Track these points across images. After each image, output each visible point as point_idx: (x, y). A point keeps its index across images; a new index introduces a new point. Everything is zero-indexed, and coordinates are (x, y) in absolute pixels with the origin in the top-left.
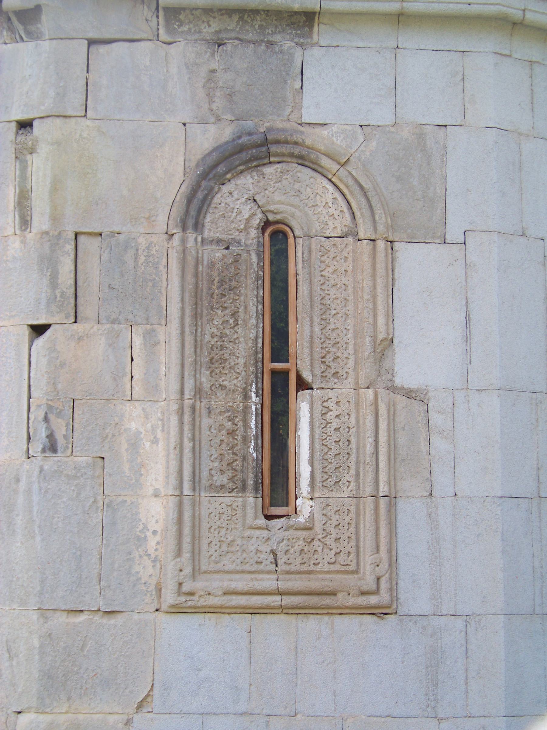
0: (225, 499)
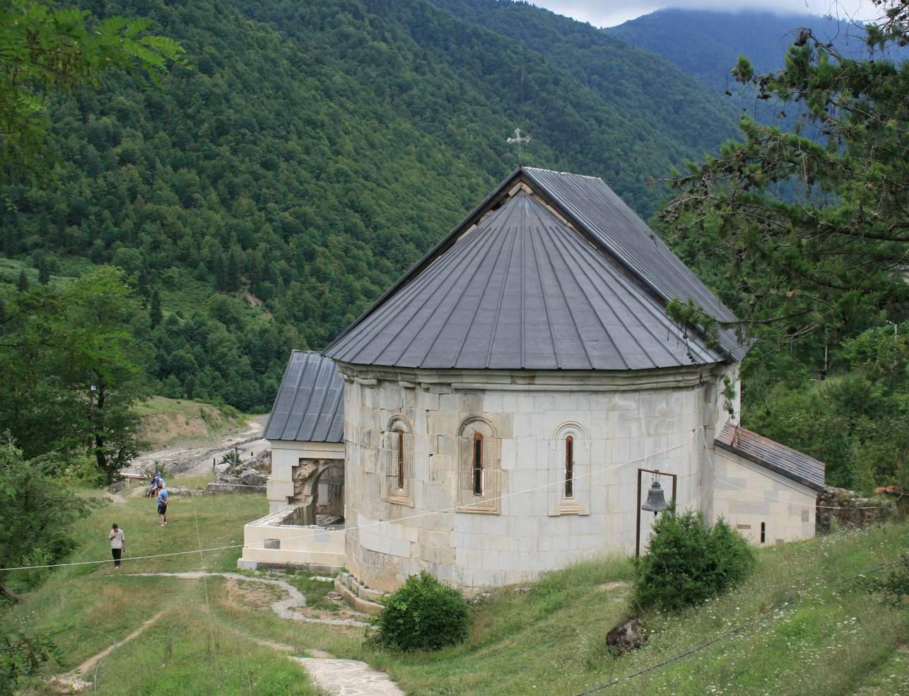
0: (467, 491)
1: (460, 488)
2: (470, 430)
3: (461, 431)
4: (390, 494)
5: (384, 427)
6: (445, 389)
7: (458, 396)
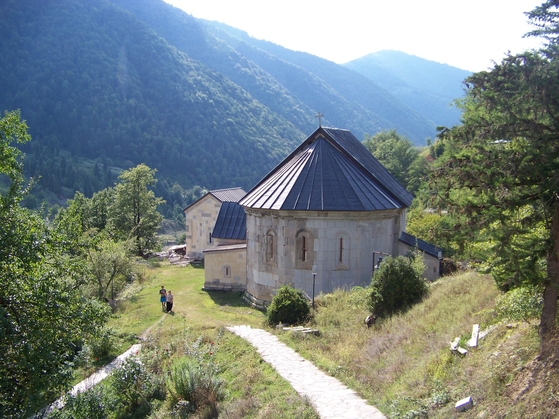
1: (297, 258)
2: (301, 235)
4: (267, 261)
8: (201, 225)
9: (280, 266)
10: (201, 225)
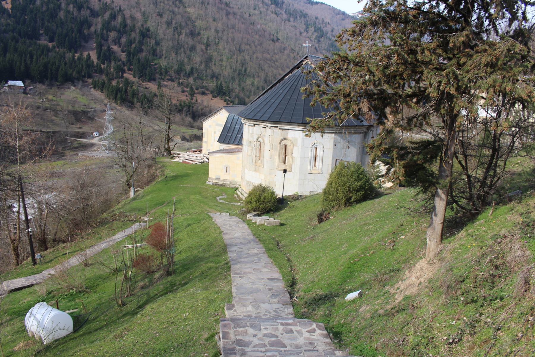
1: (279, 162)
2: (283, 142)
3: (280, 143)
4: (256, 163)
5: (255, 140)
6: (276, 128)
7: (280, 130)
8: (215, 133)
9: (265, 167)
10: (215, 133)
